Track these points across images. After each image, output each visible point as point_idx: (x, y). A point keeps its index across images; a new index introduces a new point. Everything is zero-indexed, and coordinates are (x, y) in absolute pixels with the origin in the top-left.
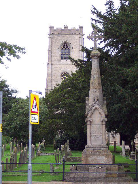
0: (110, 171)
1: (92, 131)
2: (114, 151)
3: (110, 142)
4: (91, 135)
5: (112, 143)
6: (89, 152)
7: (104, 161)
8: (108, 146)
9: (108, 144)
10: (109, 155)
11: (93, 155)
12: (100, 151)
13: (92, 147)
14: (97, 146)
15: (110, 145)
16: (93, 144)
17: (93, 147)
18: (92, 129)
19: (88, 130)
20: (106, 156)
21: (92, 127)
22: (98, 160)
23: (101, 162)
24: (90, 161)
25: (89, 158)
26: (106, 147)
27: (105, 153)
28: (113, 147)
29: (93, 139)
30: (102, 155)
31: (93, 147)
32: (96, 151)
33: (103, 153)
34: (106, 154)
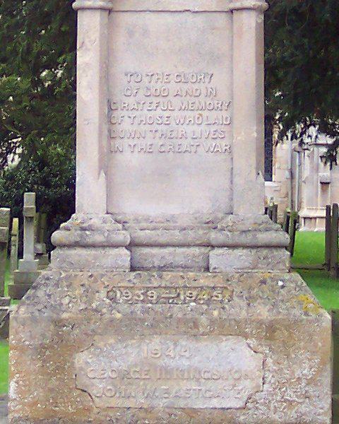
0: (287, 194)
1: (121, 82)
2: (328, 264)
3: (304, 213)
4: (109, 107)
5: (312, 214)
6: (89, 293)
7: (247, 386)
8: (284, 238)
9: (291, 223)
10: (297, 322)
11: (129, 328)
12: (204, 280)
13: (124, 237)
14: (177, 236)
15: (303, 228)
16: (132, 206)
17: (131, 246)
18: (127, 62)
19: (87, 59)
20: (269, 332)
21: (121, 40)
22: (182, 374)
23: (215, 403)
24: (98, 388)
25: (81, 359)
26: (263, 237)
27: (250, 300)
28: (322, 240)
29: (129, 159)
30: (222, 328)
31: (131, 246)
32: (165, 283)
33: (238, 309)
34: (263, 312)
